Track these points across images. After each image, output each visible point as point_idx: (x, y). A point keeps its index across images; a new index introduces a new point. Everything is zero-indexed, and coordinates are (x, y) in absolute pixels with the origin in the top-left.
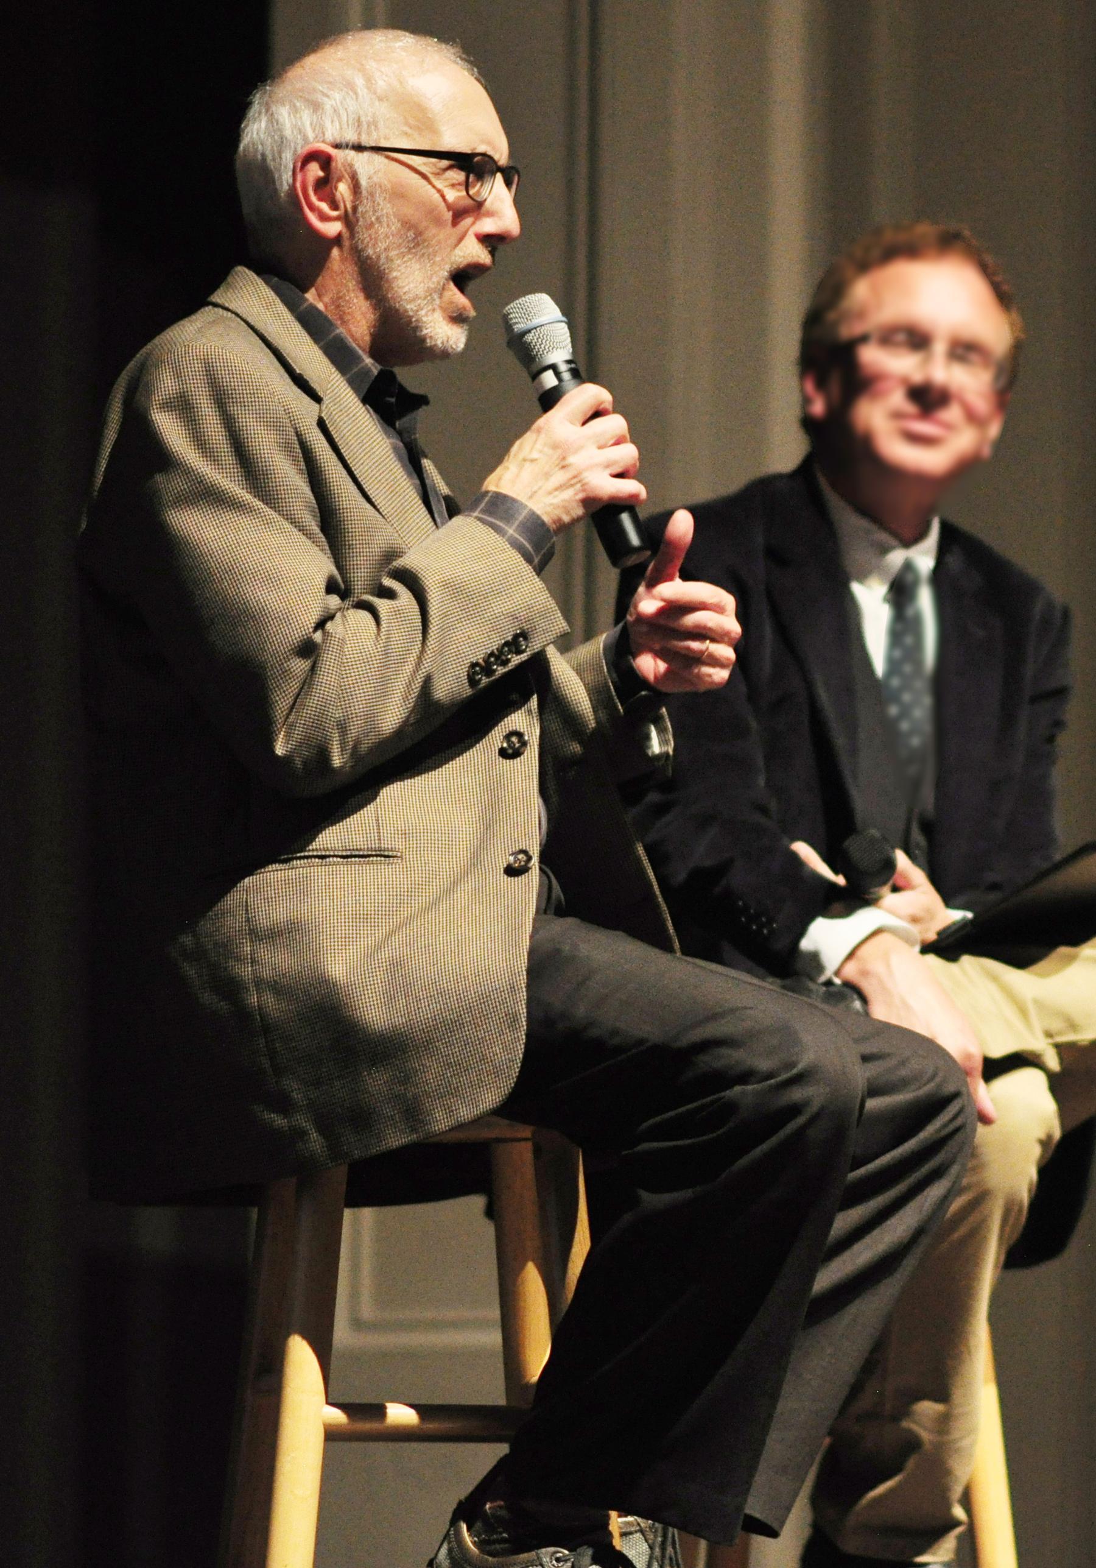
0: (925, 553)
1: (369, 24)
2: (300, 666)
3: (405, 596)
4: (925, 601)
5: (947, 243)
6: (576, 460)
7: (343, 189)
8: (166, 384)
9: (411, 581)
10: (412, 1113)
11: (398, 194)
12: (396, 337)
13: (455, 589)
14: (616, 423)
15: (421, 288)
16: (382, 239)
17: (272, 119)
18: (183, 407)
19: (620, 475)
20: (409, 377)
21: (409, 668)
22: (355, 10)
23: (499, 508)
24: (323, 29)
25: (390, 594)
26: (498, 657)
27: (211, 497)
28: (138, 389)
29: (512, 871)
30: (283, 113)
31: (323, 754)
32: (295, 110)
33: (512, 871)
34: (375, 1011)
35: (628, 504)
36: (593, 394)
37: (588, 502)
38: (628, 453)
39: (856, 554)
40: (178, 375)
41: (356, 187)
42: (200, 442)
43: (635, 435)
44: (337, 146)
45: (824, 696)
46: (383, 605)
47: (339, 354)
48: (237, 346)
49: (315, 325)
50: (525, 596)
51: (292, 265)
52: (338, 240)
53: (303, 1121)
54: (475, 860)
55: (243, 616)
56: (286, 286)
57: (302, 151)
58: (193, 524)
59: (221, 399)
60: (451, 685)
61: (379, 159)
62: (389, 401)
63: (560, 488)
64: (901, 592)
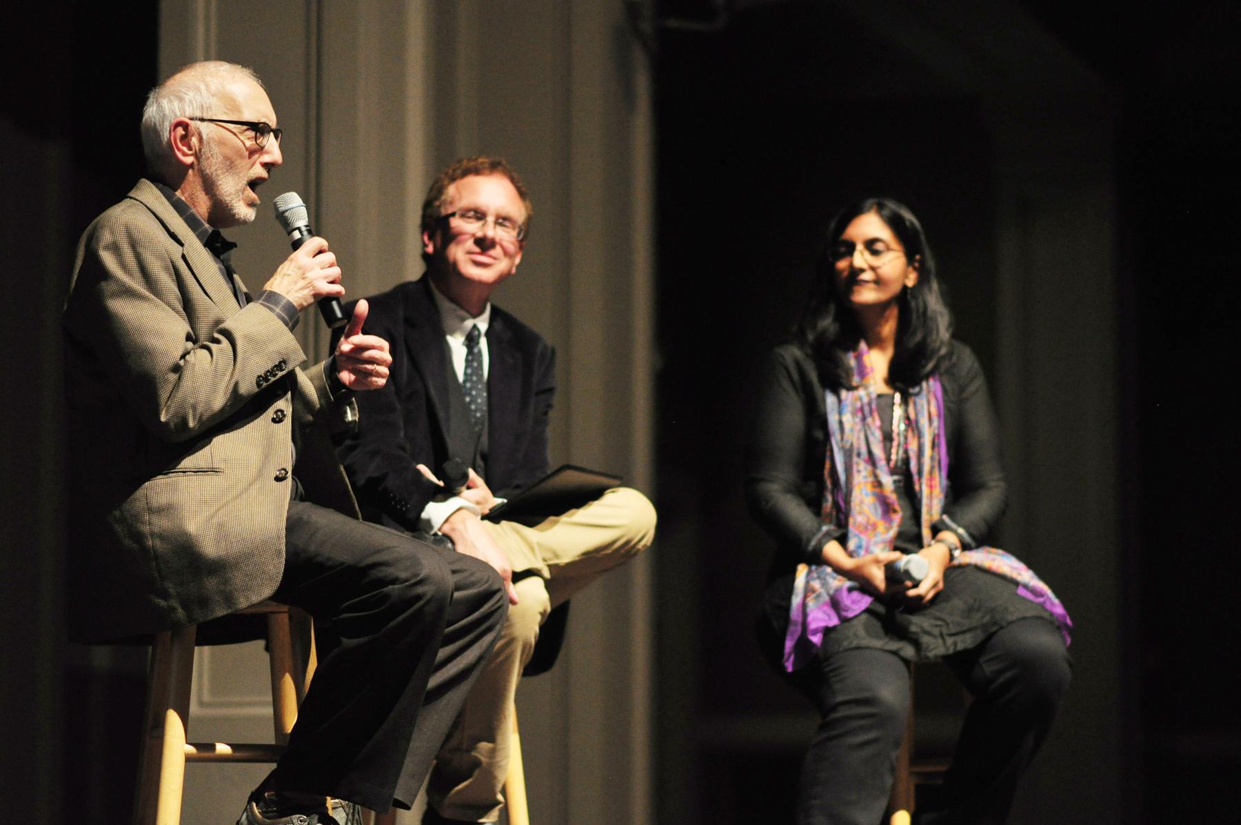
1: (207, 58)
2: (173, 377)
3: (225, 343)
7: (194, 140)
8: (106, 237)
9: (228, 334)
11: (222, 143)
13: (249, 339)
14: (330, 257)
16: (214, 165)
17: (159, 105)
18: (115, 248)
20: (227, 234)
25: (218, 341)
26: (271, 372)
27: (129, 293)
28: (93, 240)
29: (278, 479)
32: (170, 101)
33: (278, 479)
34: (210, 548)
35: (335, 297)
36: (318, 242)
38: (336, 271)
39: (449, 321)
40: (112, 233)
41: (201, 139)
43: (340, 262)
44: (191, 119)
46: (214, 347)
47: (192, 222)
48: (141, 219)
49: (180, 207)
50: (286, 342)
51: (169, 177)
52: (192, 166)
53: (175, 603)
54: (260, 474)
55: (145, 352)
56: (166, 188)
57: (174, 121)
58: (121, 308)
59: (134, 245)
60: (248, 386)
61: (212, 125)
62: (217, 245)
63: (302, 289)
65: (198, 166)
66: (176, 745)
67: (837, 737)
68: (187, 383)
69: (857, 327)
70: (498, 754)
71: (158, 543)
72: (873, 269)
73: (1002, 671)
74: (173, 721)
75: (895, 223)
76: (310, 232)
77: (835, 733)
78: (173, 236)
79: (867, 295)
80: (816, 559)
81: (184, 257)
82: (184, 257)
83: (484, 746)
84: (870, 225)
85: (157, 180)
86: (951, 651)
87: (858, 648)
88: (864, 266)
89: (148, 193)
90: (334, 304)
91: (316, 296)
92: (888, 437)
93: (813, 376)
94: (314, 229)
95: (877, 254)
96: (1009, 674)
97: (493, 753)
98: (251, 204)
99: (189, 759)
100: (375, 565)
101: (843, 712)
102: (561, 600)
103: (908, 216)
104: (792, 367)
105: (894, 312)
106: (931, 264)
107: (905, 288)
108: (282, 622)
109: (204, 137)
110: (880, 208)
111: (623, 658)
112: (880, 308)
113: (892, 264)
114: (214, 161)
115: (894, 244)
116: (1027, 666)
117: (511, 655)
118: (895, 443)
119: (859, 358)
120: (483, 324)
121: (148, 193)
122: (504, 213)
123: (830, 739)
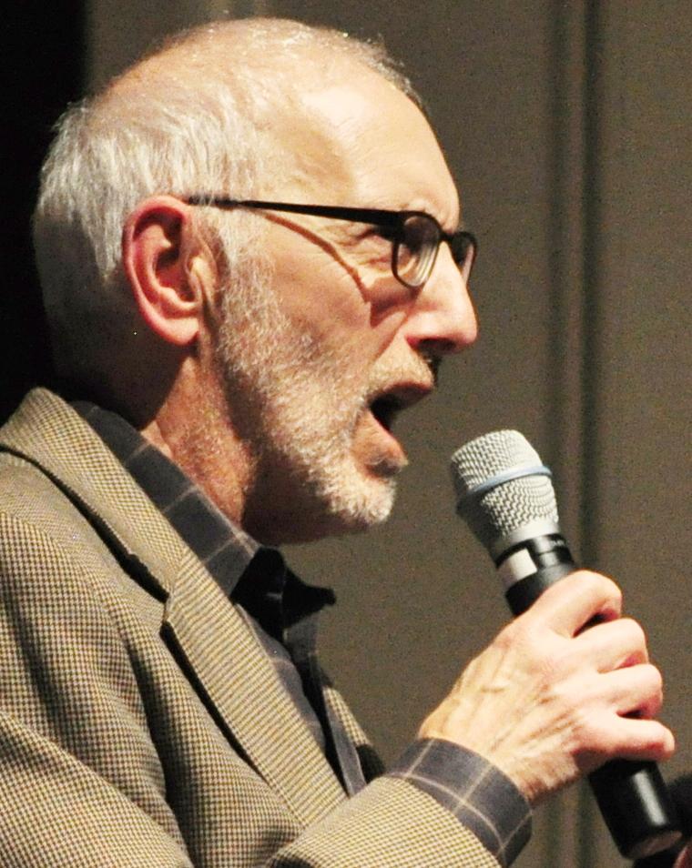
7: (200, 267)
11: (286, 275)
14: (626, 633)
16: (261, 346)
17: (90, 159)
20: (304, 561)
32: (125, 144)
36: (591, 587)
41: (220, 265)
44: (192, 201)
47: (194, 525)
49: (156, 479)
51: (118, 380)
52: (192, 347)
56: (112, 419)
57: (137, 208)
61: (256, 221)
63: (540, 734)
78: (134, 569)
81: (167, 634)
82: (167, 634)
90: (642, 781)
94: (576, 551)
109: (233, 257)
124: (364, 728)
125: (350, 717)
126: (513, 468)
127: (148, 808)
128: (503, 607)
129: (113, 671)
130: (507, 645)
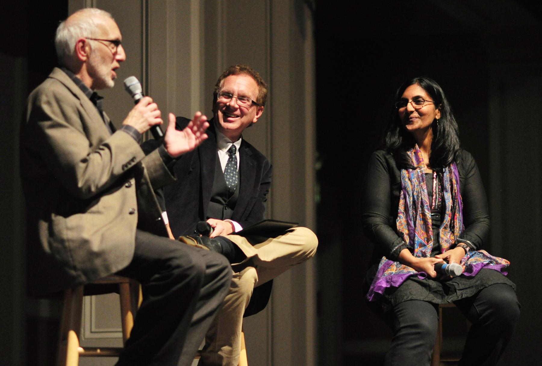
0: (238, 144)
1: (92, 7)
2: (82, 165)
3: (107, 150)
4: (238, 154)
5: (242, 70)
6: (146, 115)
7: (87, 49)
8: (44, 98)
9: (107, 146)
10: (107, 268)
11: (100, 50)
12: (98, 83)
13: (118, 147)
14: (154, 106)
15: (106, 72)
16: (96, 61)
17: (69, 30)
18: (49, 103)
19: (157, 118)
20: (100, 93)
21: (108, 168)
22: (89, 2)
23: (128, 128)
24: (81, 6)
25: (103, 149)
26: (129, 163)
27: (57, 125)
28: (36, 99)
29: (131, 213)
30: (72, 29)
31: (89, 188)
32: (75, 29)
33: (131, 213)
34: (96, 247)
35: (158, 125)
36: (148, 99)
37: (150, 125)
38: (158, 112)
39: (221, 142)
40: (47, 96)
41: (90, 48)
42: (54, 112)
43: (159, 108)
44: (86, 38)
45: (205, 171)
46: (102, 152)
47: (83, 88)
48: (57, 87)
49: (77, 82)
50: (135, 149)
51: (72, 66)
52: (85, 62)
53: (79, 273)
54: (121, 212)
55: (66, 154)
56: (69, 72)
57: (78, 40)
58: (53, 133)
59: (58, 101)
60: (118, 170)
61: (96, 42)
62: (94, 98)
63: (143, 122)
64: (231, 152)
65: (88, 62)
66: (74, 348)
67: (402, 344)
68: (90, 169)
69: (412, 140)
70: (233, 353)
71: (71, 244)
72: (417, 110)
73: (485, 310)
74: (72, 335)
75: (429, 90)
76: (143, 95)
77: (400, 342)
78: (75, 95)
79: (418, 123)
80: (397, 258)
81: (81, 105)
82: (81, 105)
83: (226, 348)
84: (416, 90)
85: (62, 66)
86: (460, 298)
87: (411, 300)
88: (413, 109)
89: (60, 75)
90: (158, 129)
91: (150, 125)
92: (430, 194)
93: (393, 162)
94: (145, 94)
95: (420, 104)
96: (489, 311)
97: (231, 353)
98: (113, 79)
99: (81, 355)
100: (170, 259)
101: (404, 332)
102: (266, 280)
103: (436, 86)
104: (383, 160)
105: (430, 131)
106: (448, 108)
107: (435, 120)
108: (126, 288)
109: (93, 48)
110: (420, 83)
111: (298, 310)
112: (423, 131)
113: (428, 107)
114: (96, 59)
115: (427, 98)
116: (497, 307)
117: (241, 303)
118: (434, 197)
119: (416, 153)
120: (238, 145)
121: (60, 75)
122: (241, 93)
123: (398, 345)
124: (109, 117)
125: (447, 212)
126: (134, 82)
127: (80, 131)
128: (134, 104)
129: (74, 111)
130: (136, 109)
